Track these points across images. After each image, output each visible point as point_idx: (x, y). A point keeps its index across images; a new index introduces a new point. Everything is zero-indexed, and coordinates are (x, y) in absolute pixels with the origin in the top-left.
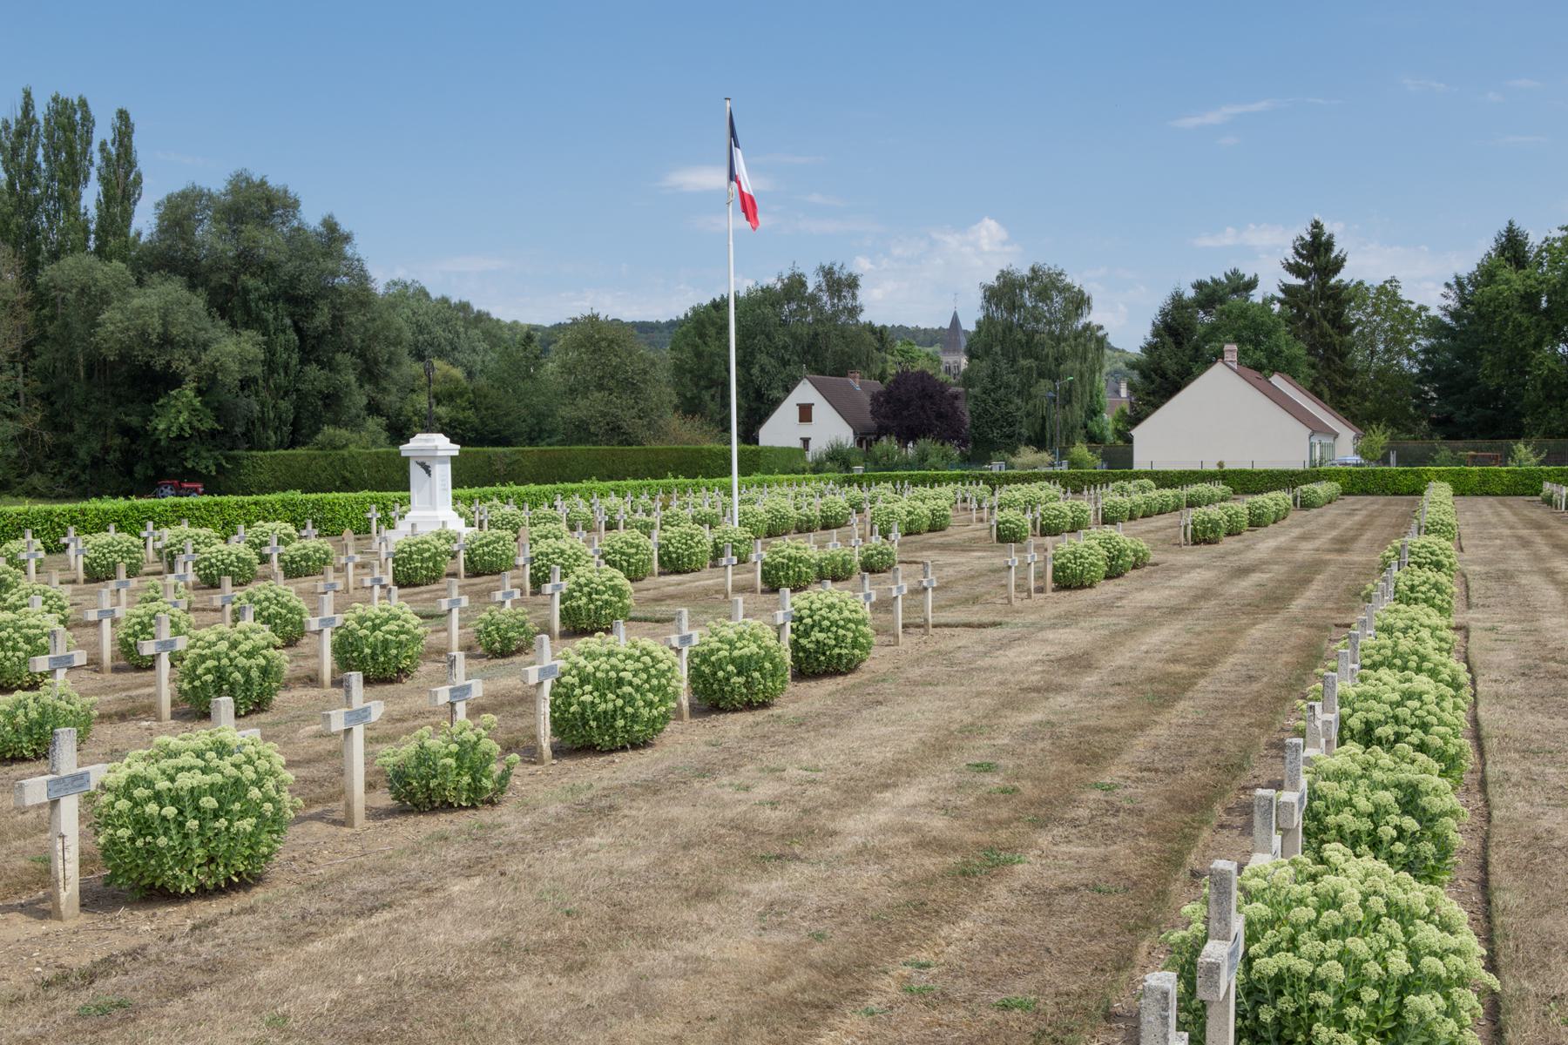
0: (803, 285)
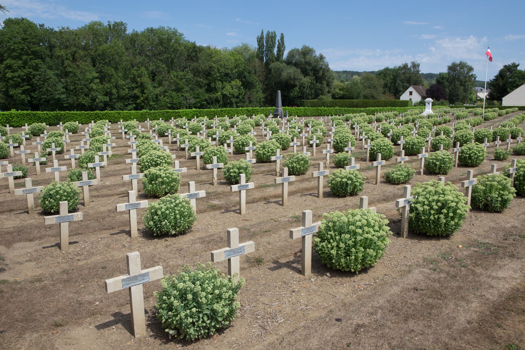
0: (408, 66)
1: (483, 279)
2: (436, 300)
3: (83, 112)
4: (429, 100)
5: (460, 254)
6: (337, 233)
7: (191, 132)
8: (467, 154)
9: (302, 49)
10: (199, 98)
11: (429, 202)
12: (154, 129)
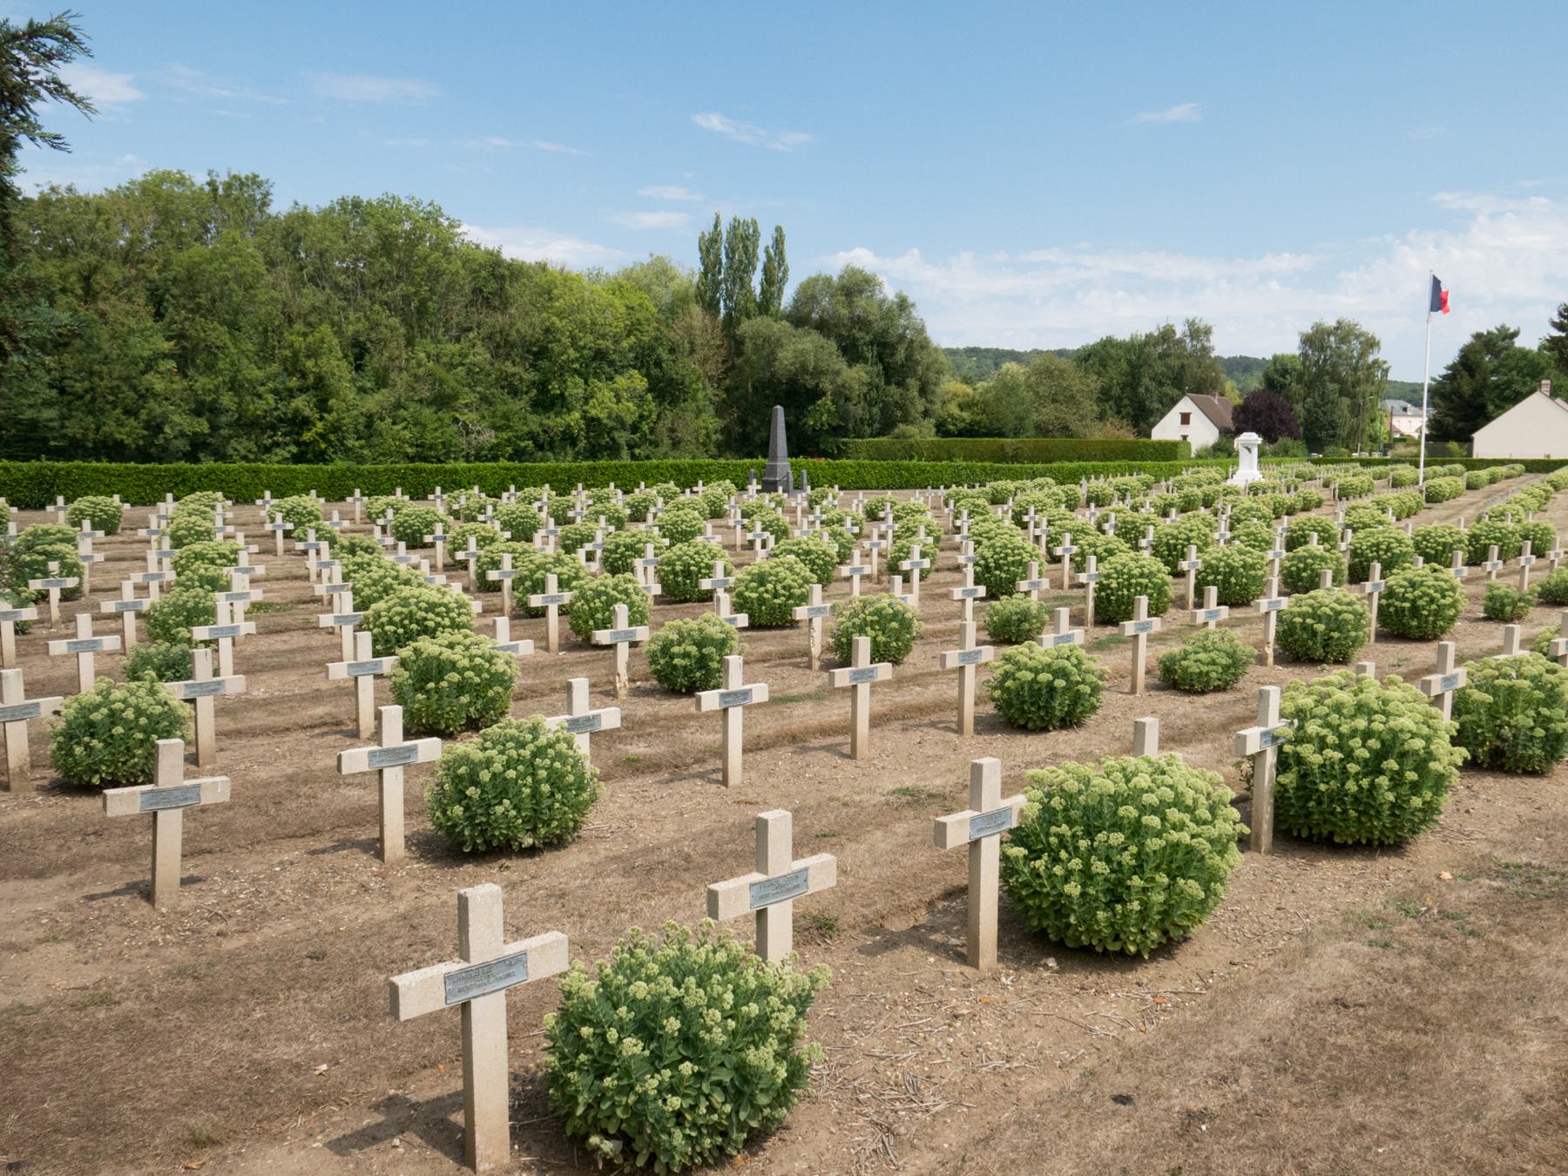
1: (1540, 970)
2: (1413, 1034)
3: (132, 464)
4: (1251, 438)
5: (1452, 897)
6: (1079, 830)
7: (508, 535)
8: (1405, 600)
9: (842, 277)
10: (509, 427)
11: (1341, 736)
12: (381, 522)
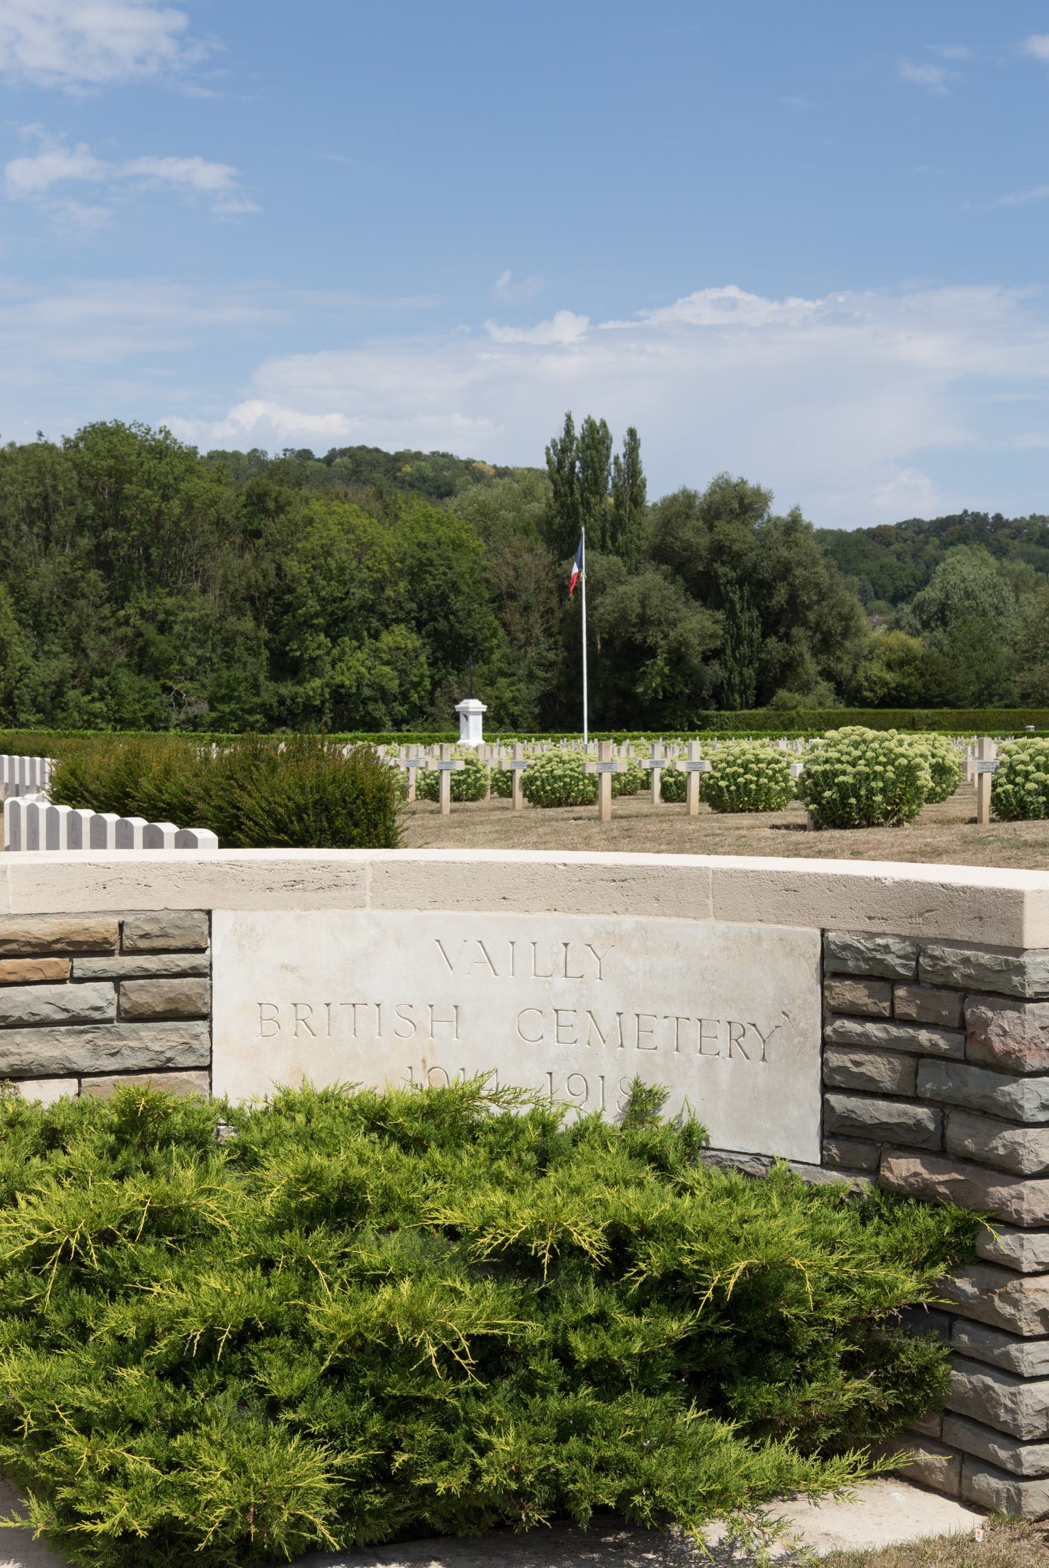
9: (712, 493)
